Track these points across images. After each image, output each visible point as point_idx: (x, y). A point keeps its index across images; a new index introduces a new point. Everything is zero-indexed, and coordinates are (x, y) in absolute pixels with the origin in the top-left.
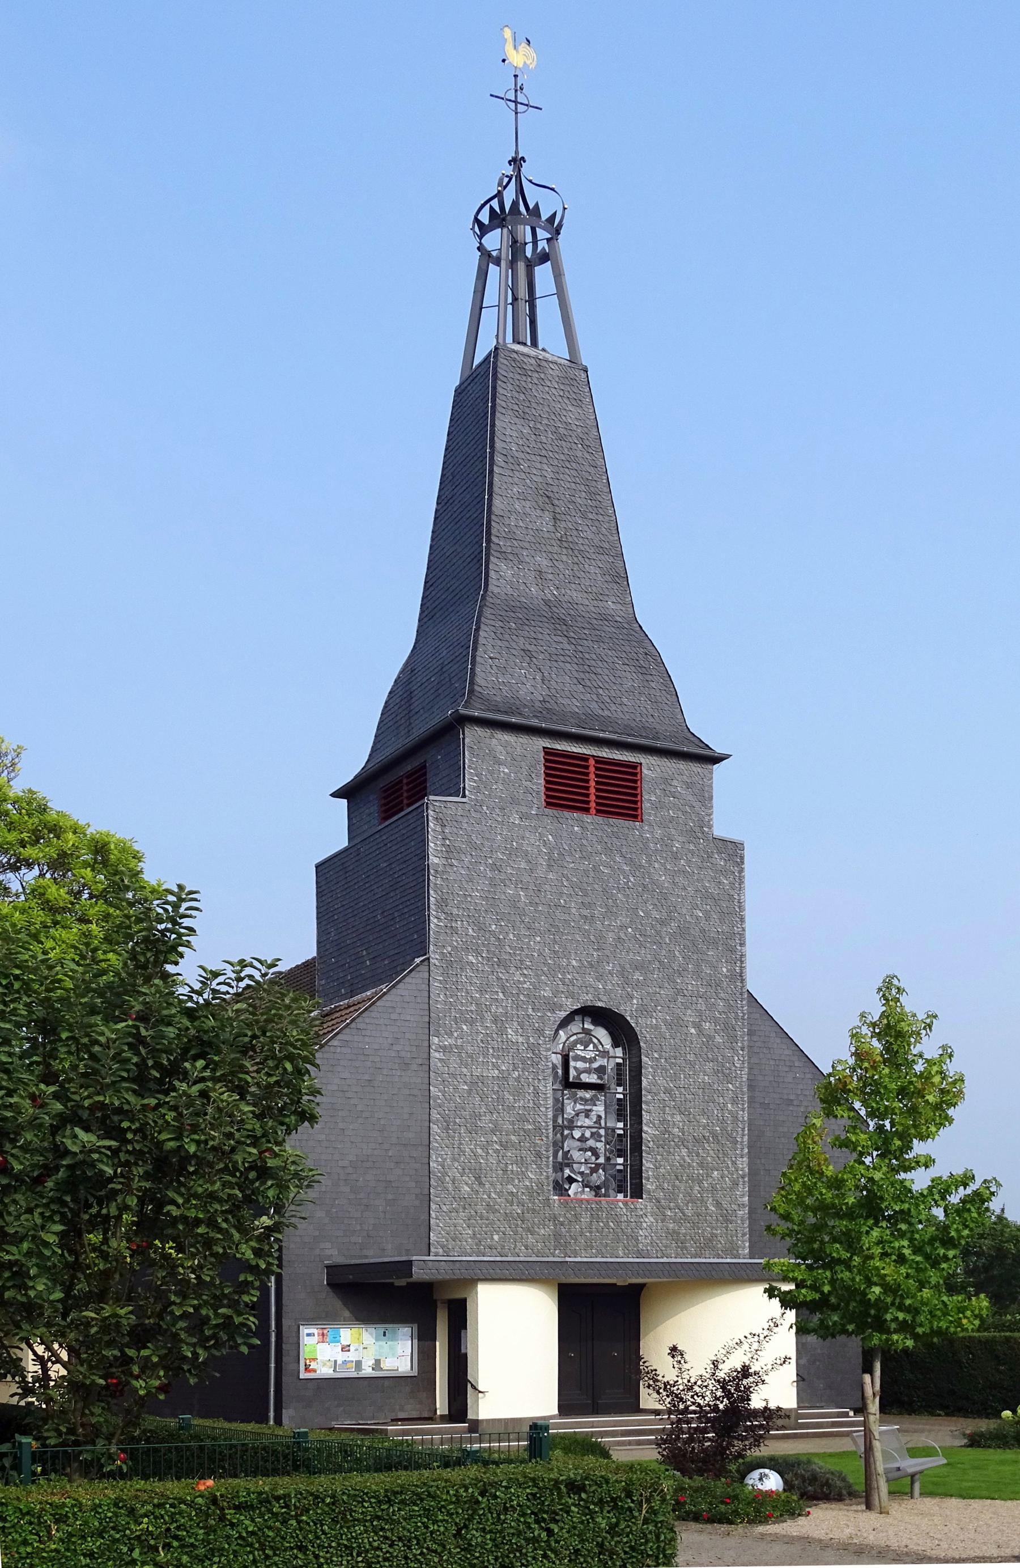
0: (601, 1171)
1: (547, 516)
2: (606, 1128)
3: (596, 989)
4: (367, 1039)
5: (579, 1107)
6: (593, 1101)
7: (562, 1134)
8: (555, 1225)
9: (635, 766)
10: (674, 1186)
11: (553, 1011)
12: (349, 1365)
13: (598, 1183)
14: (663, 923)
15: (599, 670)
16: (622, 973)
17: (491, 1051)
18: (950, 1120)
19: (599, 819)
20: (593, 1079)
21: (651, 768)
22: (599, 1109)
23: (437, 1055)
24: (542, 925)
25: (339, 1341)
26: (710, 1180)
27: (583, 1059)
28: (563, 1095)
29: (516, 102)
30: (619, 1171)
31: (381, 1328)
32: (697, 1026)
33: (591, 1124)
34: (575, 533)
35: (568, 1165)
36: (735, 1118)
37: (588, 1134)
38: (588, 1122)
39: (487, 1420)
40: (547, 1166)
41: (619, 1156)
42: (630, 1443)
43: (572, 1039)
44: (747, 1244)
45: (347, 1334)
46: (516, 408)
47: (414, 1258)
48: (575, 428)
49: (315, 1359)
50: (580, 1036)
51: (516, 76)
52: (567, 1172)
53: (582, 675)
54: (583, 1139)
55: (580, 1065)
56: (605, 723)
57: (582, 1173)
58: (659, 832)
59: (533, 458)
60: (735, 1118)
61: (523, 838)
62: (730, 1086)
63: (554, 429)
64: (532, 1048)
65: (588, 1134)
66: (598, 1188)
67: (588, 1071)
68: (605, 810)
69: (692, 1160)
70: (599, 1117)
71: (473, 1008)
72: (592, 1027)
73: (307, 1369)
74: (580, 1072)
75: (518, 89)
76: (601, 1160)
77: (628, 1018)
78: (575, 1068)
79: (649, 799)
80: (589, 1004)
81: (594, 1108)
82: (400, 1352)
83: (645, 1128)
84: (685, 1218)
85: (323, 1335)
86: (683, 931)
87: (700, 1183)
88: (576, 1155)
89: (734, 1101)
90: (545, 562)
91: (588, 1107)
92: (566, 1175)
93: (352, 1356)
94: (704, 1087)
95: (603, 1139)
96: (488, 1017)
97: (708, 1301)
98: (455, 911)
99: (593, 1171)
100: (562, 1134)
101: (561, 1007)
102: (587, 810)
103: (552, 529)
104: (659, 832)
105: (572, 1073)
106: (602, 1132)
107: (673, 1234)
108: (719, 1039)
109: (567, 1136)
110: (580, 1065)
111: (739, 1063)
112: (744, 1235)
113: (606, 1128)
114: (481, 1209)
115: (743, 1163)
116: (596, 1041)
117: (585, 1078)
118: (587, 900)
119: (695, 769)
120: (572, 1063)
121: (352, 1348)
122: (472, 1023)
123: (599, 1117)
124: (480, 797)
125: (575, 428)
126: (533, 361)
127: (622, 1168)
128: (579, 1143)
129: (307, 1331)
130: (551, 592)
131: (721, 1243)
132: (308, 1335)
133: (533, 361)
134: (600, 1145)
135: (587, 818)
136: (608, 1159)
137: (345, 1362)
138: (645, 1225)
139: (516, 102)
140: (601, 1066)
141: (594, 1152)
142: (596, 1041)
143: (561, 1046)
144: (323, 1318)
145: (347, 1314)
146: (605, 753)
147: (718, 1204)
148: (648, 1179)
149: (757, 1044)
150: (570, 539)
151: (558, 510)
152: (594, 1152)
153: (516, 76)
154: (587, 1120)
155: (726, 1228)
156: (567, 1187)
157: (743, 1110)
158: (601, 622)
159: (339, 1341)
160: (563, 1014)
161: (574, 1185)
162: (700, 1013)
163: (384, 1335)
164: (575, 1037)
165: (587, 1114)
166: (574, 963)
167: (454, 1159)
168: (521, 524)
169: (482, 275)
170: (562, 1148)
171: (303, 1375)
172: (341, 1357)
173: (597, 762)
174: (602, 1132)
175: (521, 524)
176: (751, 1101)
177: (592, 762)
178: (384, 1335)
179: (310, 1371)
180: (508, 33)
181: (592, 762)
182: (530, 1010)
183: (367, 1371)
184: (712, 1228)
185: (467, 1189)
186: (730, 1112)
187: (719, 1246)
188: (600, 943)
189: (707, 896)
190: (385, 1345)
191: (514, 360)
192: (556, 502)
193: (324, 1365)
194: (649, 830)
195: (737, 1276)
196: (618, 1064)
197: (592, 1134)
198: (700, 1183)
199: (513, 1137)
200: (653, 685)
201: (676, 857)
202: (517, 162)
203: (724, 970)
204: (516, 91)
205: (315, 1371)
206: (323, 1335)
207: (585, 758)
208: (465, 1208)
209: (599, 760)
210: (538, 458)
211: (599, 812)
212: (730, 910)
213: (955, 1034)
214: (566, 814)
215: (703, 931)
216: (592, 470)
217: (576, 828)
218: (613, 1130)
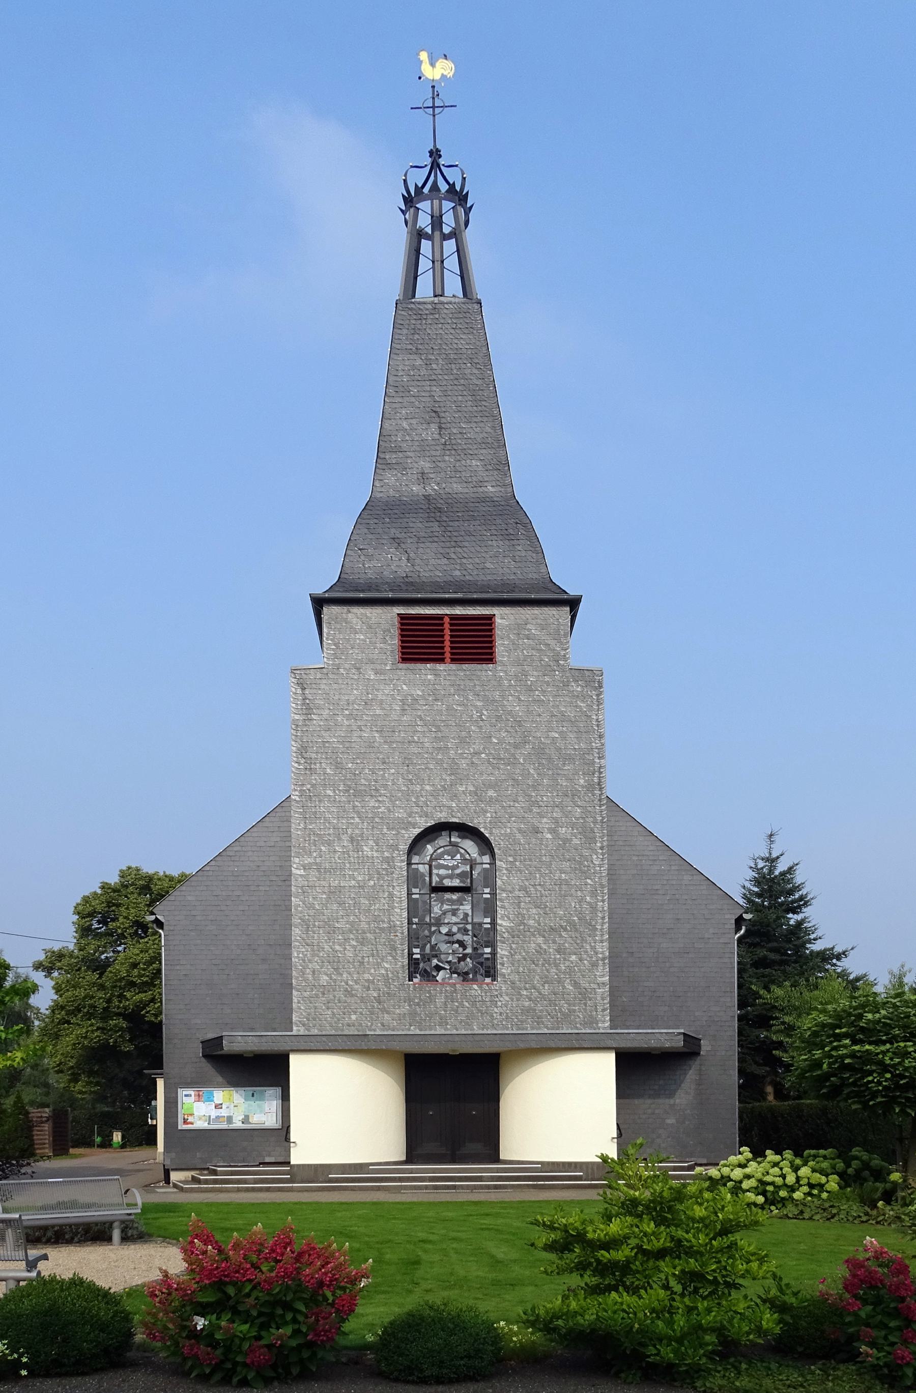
0: (468, 959)
1: (434, 427)
2: (473, 924)
3: (450, 807)
4: (236, 864)
5: (445, 907)
6: (460, 902)
7: (430, 931)
8: (410, 1006)
9: (491, 618)
10: (529, 970)
11: (406, 829)
12: (221, 1120)
13: (466, 970)
14: (516, 746)
15: (466, 544)
17: (348, 865)
18: (123, 875)
19: (454, 666)
20: (456, 883)
21: (503, 617)
22: (467, 908)
23: (298, 872)
24: (397, 758)
25: (213, 1101)
26: (567, 963)
27: (446, 867)
28: (430, 898)
29: (433, 107)
30: (487, 959)
31: (250, 1089)
32: (553, 831)
33: (458, 920)
34: (459, 436)
35: (436, 956)
36: (594, 909)
37: (455, 929)
38: (454, 919)
39: (298, 1165)
40: (403, 957)
41: (487, 947)
42: (426, 1187)
43: (439, 851)
44: (608, 1018)
45: (219, 1095)
46: (410, 347)
47: (224, 1034)
48: (465, 351)
49: (192, 1115)
50: (446, 848)
51: (433, 87)
52: (435, 962)
53: (447, 550)
54: (450, 934)
55: (442, 872)
56: (513, 588)
57: (449, 962)
58: (513, 670)
59: (424, 383)
61: (377, 690)
62: (589, 881)
63: (444, 356)
64: (387, 860)
65: (455, 929)
66: (467, 973)
67: (451, 877)
68: (459, 658)
69: (549, 947)
70: (466, 915)
71: (331, 831)
72: (459, 840)
73: (185, 1122)
74: (442, 878)
75: (435, 96)
76: (469, 950)
77: (482, 830)
78: (438, 875)
80: (443, 820)
81: (461, 907)
82: (267, 1109)
83: (499, 921)
84: (543, 997)
85: (199, 1095)
86: (540, 751)
87: (557, 966)
88: (443, 947)
89: (594, 894)
90: (428, 465)
91: (454, 907)
92: (434, 964)
93: (224, 1112)
94: (560, 883)
95: (470, 933)
97: (534, 1068)
98: (314, 756)
99: (463, 958)
100: (430, 931)
101: (414, 826)
102: (442, 661)
103: (437, 437)
104: (513, 670)
105: (435, 879)
106: (469, 927)
107: (527, 1011)
108: (576, 841)
109: (434, 932)
110: (442, 872)
111: (598, 861)
112: (604, 1010)
113: (473, 924)
114: (340, 994)
115: (603, 949)
116: (462, 851)
117: (447, 883)
118: (440, 735)
119: (549, 612)
120: (435, 871)
121: (224, 1106)
122: (329, 843)
123: (466, 915)
124: (337, 662)
125: (465, 351)
126: (430, 306)
127: (489, 956)
128: (447, 938)
129: (184, 1093)
130: (432, 488)
132: (186, 1096)
133: (430, 306)
135: (440, 667)
136: (475, 949)
137: (218, 1117)
138: (499, 1004)
139: (433, 107)
140: (463, 872)
141: (462, 944)
142: (462, 851)
143: (428, 858)
144: (197, 1082)
145: (220, 1079)
146: (458, 611)
147: (576, 984)
148: (503, 964)
149: (617, 843)
150: (454, 442)
151: (443, 420)
152: (462, 944)
153: (433, 87)
154: (454, 918)
155: (585, 1004)
156: (435, 974)
157: (603, 901)
158: (477, 505)
159: (213, 1101)
160: (417, 831)
161: (441, 973)
162: (556, 821)
163: (253, 1095)
164: (442, 849)
165: (454, 913)
166: (428, 788)
167: (313, 955)
168: (407, 438)
169: (415, 253)
170: (430, 942)
171: (181, 1126)
172: (214, 1113)
173: (451, 619)
174: (469, 927)
175: (407, 438)
176: (611, 894)
177: (447, 620)
178: (253, 1095)
179: (188, 1124)
180: (424, 56)
181: (447, 620)
182: (385, 830)
183: (237, 1124)
184: (569, 1005)
185: (326, 978)
186: (589, 903)
187: (578, 1020)
188: (454, 769)
189: (563, 718)
190: (253, 1104)
191: (411, 309)
192: (442, 415)
193: (200, 1119)
196: (485, 870)
197: (459, 929)
199: (368, 935)
200: (519, 548)
201: (530, 689)
202: (435, 154)
203: (582, 781)
204: (433, 98)
205: (192, 1123)
206: (199, 1095)
207: (440, 617)
208: (324, 994)
209: (453, 618)
210: (428, 383)
211: (453, 660)
212: (590, 730)
215: (559, 749)
216: (479, 382)
217: (429, 677)
218: (480, 924)
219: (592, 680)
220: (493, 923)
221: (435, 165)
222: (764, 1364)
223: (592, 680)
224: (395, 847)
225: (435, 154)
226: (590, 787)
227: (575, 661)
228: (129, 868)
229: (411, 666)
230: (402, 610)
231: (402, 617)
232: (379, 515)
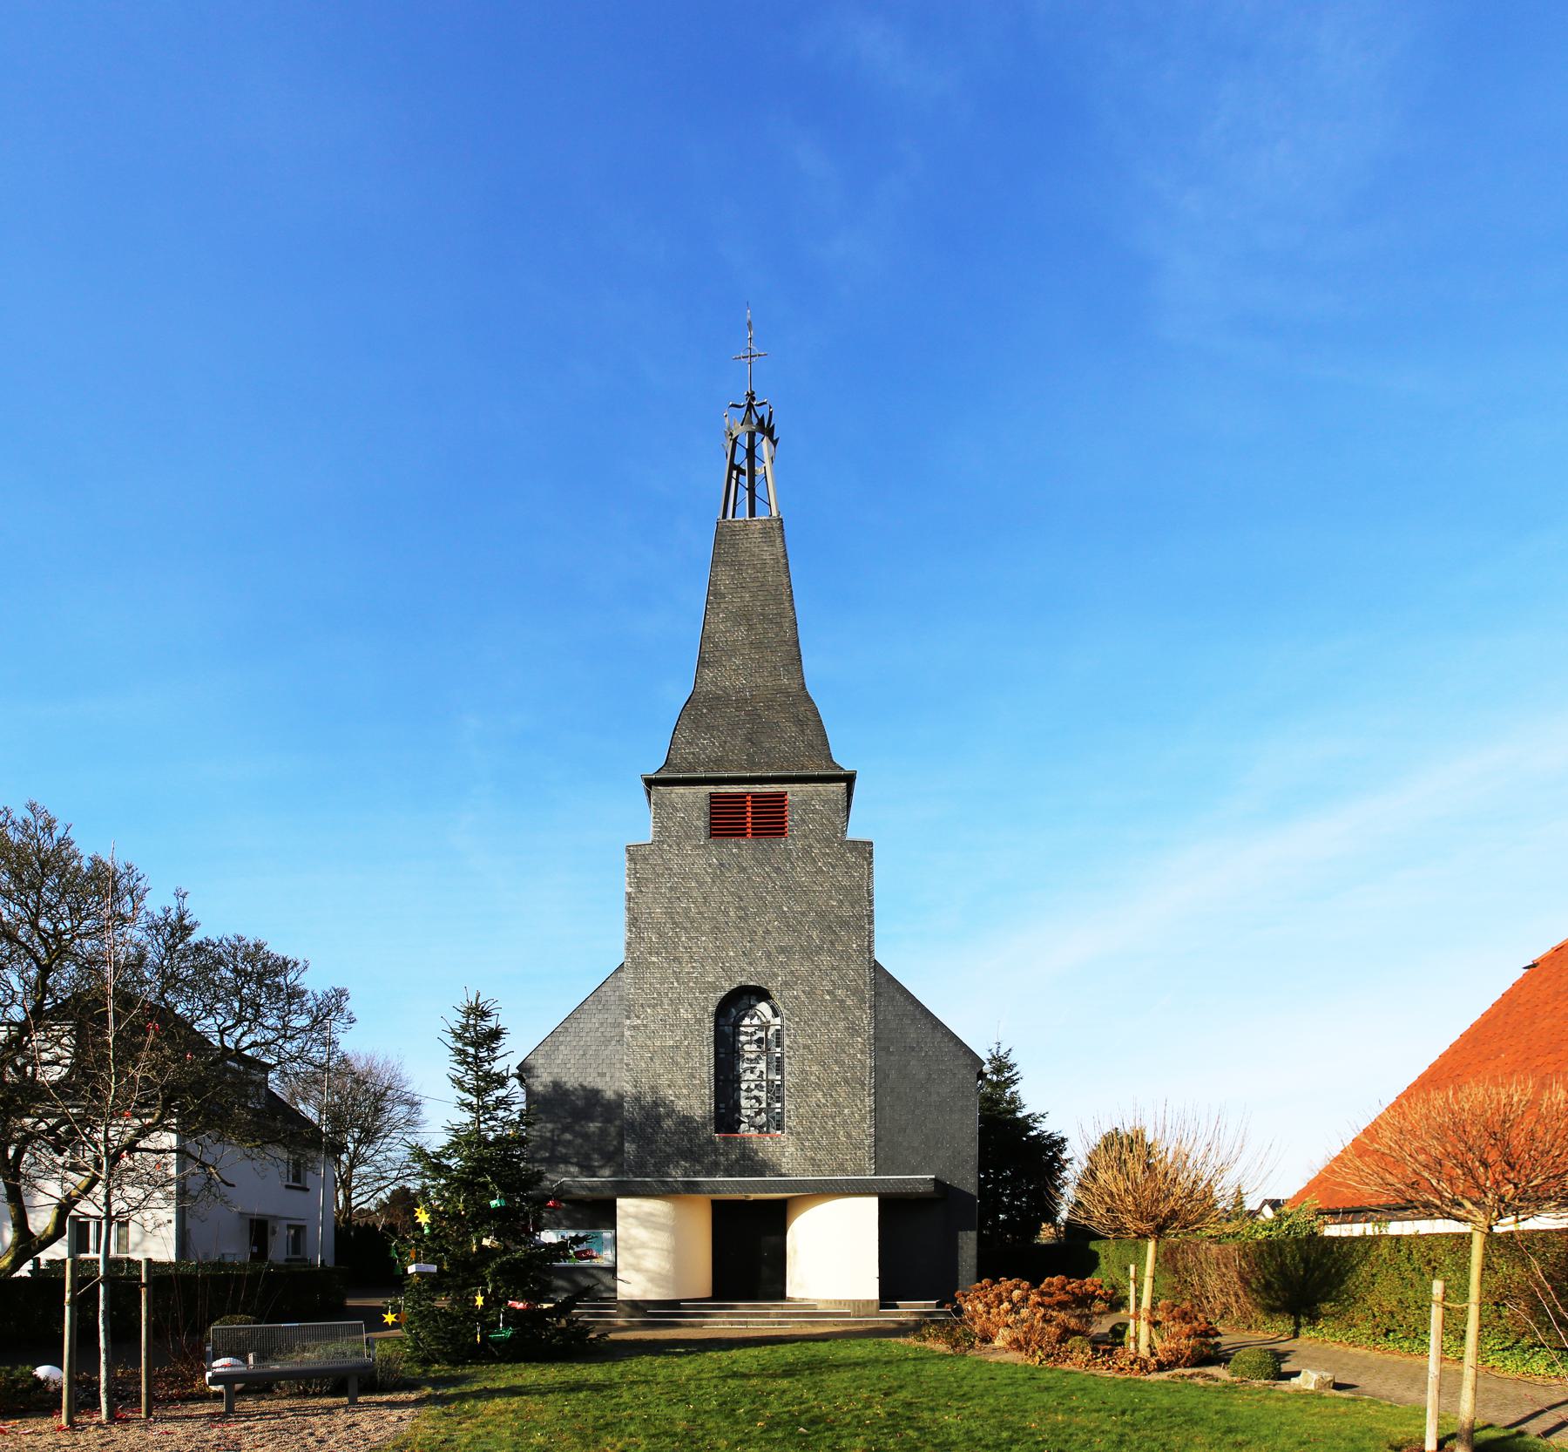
9: (783, 795)
14: (803, 914)
16: (769, 955)
21: (793, 792)
36: (863, 1067)
38: (753, 1077)
54: (749, 1090)
60: (863, 1067)
68: (757, 833)
79: (792, 818)
87: (833, 1118)
96: (666, 1001)
99: (758, 1113)
108: (849, 1002)
111: (865, 1019)
122: (654, 1006)
131: (850, 1166)
134: (763, 1095)
135: (743, 841)
141: (757, 1099)
147: (849, 1136)
152: (757, 1099)
165: (752, 1070)
194: (792, 843)
195: (173, 1131)
198: (833, 1118)
202: (751, 396)
207: (743, 796)
213: (241, 933)
214: (725, 839)
219: (864, 850)
220: (782, 1080)
221: (750, 407)
222: (998, 1343)
223: (864, 850)
224: (705, 1009)
225: (751, 396)
226: (860, 952)
227: (851, 835)
228: (240, 939)
229: (719, 840)
230: (712, 789)
231: (712, 796)
232: (696, 711)
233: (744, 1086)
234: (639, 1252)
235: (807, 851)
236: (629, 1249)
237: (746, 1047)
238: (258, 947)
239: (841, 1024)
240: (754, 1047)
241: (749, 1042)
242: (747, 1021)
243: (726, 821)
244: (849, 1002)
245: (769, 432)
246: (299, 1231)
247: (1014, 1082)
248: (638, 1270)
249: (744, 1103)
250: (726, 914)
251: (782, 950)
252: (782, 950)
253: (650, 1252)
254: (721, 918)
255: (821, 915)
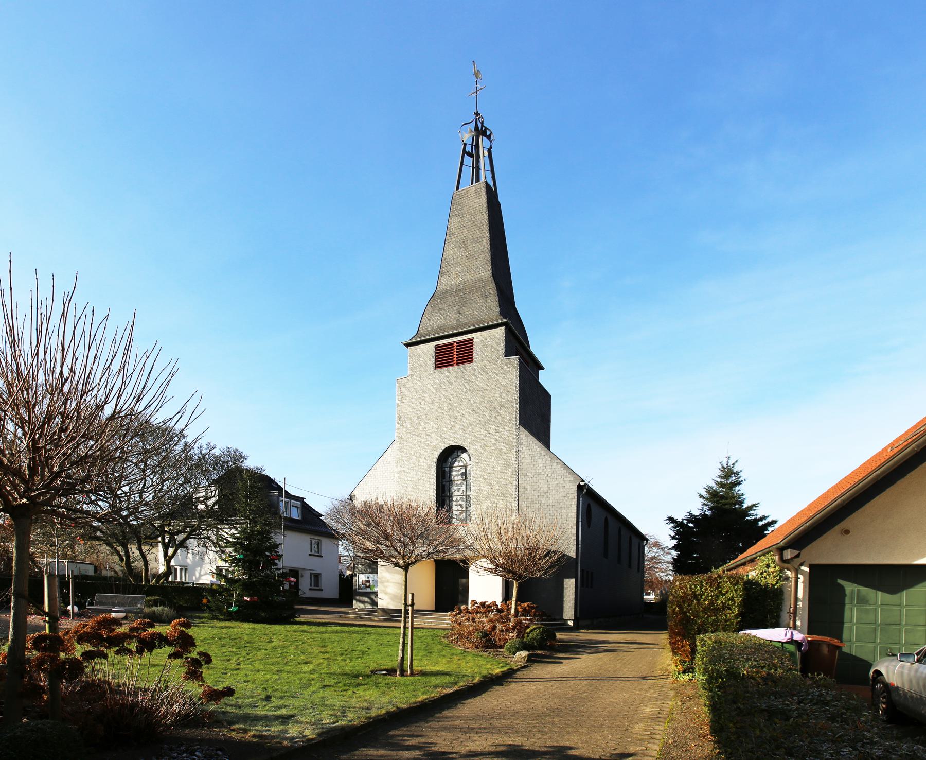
9: (472, 339)
38: (459, 494)
54: (457, 501)
99: (461, 513)
108: (505, 450)
141: (461, 505)
152: (461, 505)
207: (452, 344)
231: (437, 347)
233: (454, 499)
234: (386, 584)
235: (484, 368)
236: (382, 583)
237: (456, 478)
238: (235, 451)
239: (500, 462)
240: (460, 478)
241: (457, 475)
242: (456, 464)
243: (443, 359)
244: (505, 450)
245: (484, 133)
246: (316, 577)
247: (739, 483)
248: (386, 593)
249: (454, 508)
250: (442, 407)
251: (470, 425)
252: (470, 425)
253: (391, 585)
254: (440, 411)
255: (491, 402)
